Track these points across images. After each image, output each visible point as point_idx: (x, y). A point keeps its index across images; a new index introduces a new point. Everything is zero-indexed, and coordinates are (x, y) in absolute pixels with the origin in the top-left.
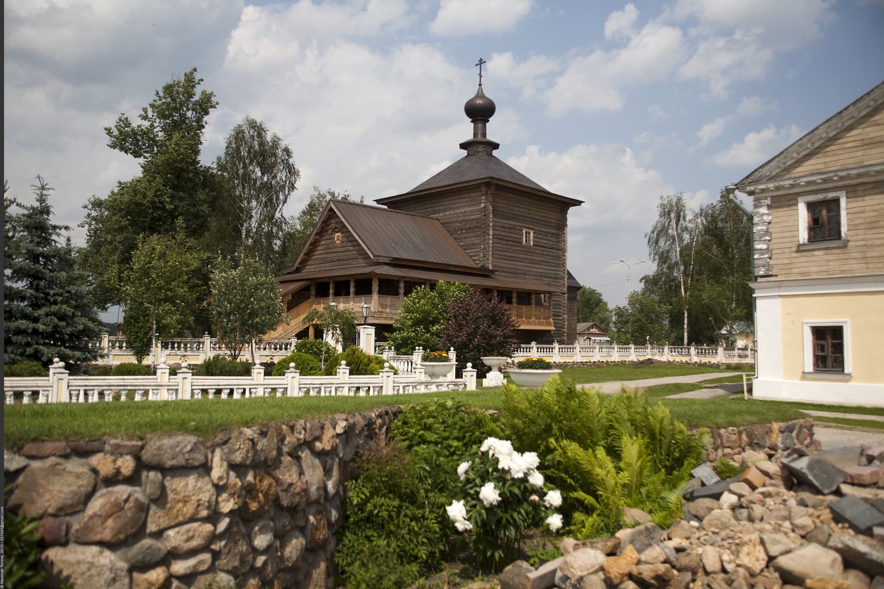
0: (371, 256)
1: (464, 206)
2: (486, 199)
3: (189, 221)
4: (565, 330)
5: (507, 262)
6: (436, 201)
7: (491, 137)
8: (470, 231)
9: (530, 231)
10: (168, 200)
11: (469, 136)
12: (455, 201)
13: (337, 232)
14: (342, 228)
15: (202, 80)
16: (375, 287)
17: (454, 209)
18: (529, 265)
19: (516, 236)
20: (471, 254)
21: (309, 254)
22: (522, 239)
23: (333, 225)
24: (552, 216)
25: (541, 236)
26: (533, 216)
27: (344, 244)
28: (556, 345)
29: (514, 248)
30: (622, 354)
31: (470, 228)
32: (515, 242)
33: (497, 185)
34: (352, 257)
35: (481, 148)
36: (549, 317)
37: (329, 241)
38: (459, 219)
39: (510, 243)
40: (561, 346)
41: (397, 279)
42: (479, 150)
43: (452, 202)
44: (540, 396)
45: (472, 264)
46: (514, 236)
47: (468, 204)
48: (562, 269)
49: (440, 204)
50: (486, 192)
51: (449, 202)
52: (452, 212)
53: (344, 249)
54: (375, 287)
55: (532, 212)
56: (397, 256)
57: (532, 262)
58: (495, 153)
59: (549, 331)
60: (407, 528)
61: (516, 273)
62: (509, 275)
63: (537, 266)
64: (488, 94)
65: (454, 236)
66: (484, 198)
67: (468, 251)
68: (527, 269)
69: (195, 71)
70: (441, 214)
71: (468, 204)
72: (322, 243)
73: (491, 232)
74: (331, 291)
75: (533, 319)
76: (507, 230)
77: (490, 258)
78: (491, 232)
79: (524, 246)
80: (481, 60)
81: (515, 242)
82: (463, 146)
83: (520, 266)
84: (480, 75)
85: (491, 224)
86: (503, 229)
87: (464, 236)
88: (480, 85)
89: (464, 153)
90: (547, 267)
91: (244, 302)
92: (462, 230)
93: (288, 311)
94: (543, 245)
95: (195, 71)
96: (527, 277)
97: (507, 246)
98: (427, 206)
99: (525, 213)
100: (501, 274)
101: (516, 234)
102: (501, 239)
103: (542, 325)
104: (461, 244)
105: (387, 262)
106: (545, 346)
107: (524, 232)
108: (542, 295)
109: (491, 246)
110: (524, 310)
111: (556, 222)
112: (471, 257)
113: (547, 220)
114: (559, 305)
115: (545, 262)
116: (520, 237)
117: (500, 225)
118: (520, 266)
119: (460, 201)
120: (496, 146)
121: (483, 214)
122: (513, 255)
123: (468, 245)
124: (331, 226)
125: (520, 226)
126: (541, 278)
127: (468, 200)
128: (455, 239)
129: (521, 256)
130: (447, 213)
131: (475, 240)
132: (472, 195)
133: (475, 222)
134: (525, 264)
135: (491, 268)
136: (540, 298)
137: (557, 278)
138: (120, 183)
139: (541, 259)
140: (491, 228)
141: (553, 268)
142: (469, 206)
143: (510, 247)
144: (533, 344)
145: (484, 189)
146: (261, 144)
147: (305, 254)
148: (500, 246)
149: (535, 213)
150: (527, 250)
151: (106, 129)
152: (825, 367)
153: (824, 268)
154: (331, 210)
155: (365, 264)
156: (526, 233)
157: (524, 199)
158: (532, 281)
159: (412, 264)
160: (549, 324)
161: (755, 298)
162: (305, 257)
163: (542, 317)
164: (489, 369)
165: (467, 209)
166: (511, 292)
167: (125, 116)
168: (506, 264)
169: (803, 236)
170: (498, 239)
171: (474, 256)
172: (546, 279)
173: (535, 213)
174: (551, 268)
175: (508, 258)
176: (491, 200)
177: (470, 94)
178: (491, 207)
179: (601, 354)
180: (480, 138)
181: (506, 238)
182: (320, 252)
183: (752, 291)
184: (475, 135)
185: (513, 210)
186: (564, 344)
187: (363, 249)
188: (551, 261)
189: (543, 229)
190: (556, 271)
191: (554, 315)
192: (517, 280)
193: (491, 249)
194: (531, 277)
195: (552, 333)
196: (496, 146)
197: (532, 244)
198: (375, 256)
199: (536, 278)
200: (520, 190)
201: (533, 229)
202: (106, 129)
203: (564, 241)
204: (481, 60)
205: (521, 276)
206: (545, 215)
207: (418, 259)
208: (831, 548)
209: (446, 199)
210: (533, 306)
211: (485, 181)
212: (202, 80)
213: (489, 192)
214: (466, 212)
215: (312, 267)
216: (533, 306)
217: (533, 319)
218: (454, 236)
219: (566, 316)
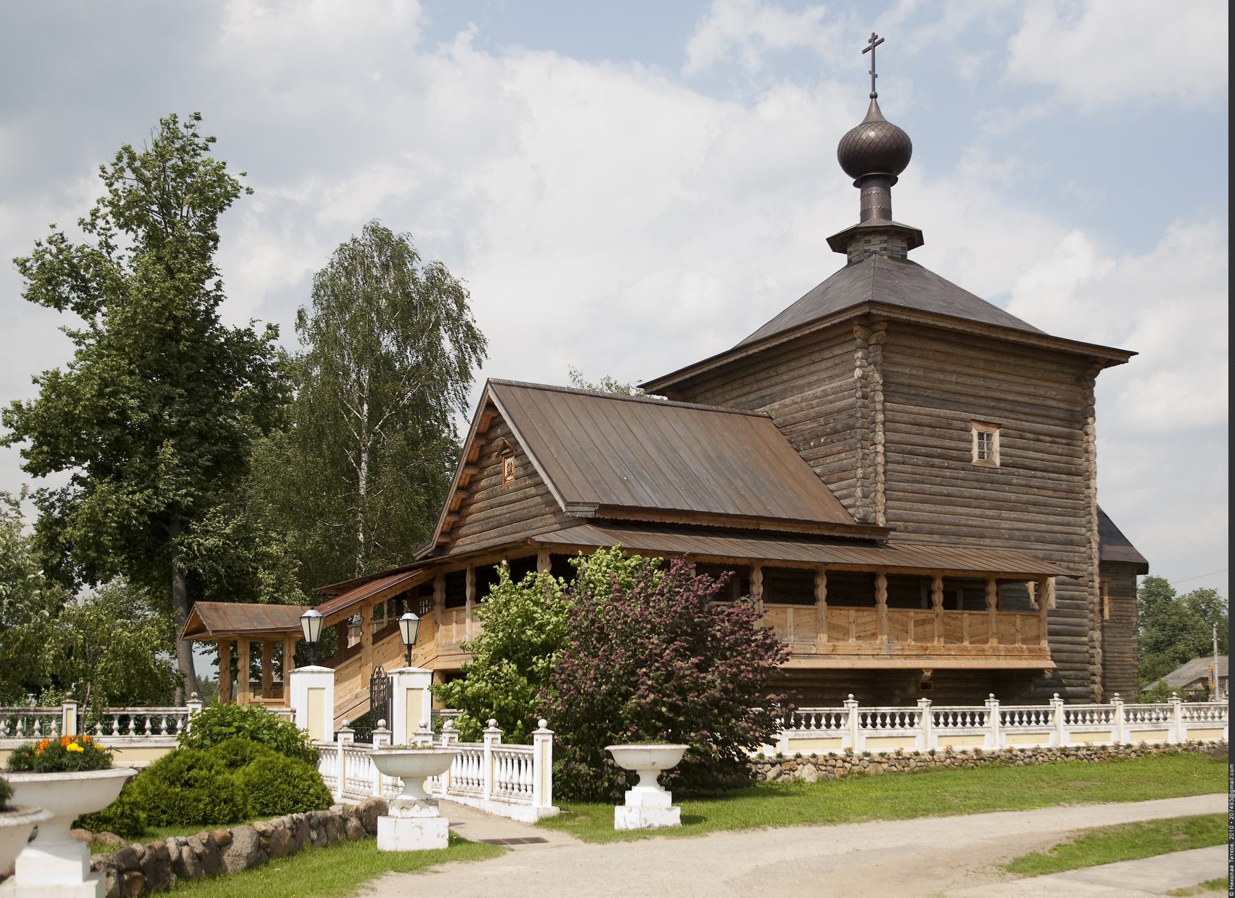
0: (561, 504)
1: (820, 381)
2: (865, 358)
4: (1097, 668)
5: (927, 506)
6: (764, 374)
7: (901, 216)
8: (835, 437)
9: (990, 430)
10: (133, 403)
11: (848, 216)
12: (804, 371)
13: (507, 456)
14: (512, 449)
15: (213, 140)
17: (801, 389)
18: (991, 513)
19: (953, 444)
20: (837, 494)
21: (460, 511)
22: (970, 450)
23: (499, 442)
24: (1052, 393)
25: (1020, 442)
26: (998, 395)
27: (521, 483)
28: (1057, 706)
29: (948, 473)
30: (1199, 725)
31: (836, 432)
32: (952, 458)
33: (891, 321)
34: (533, 511)
35: (876, 244)
36: (1038, 638)
37: (494, 479)
38: (812, 412)
39: (937, 461)
40: (869, 710)
41: (747, 562)
42: (873, 248)
43: (795, 374)
45: (840, 517)
46: (947, 443)
47: (829, 373)
48: (1084, 521)
49: (773, 381)
50: (866, 340)
51: (791, 374)
52: (797, 398)
53: (520, 494)
55: (995, 384)
57: (999, 504)
58: (913, 255)
59: (1040, 672)
61: (955, 534)
62: (936, 538)
63: (1013, 515)
65: (803, 453)
66: (859, 354)
67: (832, 487)
68: (987, 522)
69: (198, 118)
70: (776, 405)
71: (829, 373)
72: (483, 483)
73: (880, 437)
75: (993, 642)
76: (927, 430)
77: (880, 498)
78: (880, 437)
79: (975, 469)
80: (875, 37)
81: (952, 458)
82: (839, 243)
83: (964, 515)
84: (875, 76)
85: (880, 417)
86: (915, 429)
87: (822, 450)
88: (874, 96)
89: (841, 260)
90: (1043, 517)
92: (818, 437)
93: (373, 644)
94: (1028, 462)
95: (198, 118)
96: (988, 541)
97: (928, 470)
98: (747, 389)
99: (975, 386)
100: (913, 536)
101: (951, 439)
102: (910, 453)
103: (1020, 657)
104: (818, 470)
105: (590, 515)
106: (1024, 708)
107: (975, 433)
108: (1031, 585)
109: (880, 469)
110: (966, 623)
111: (1062, 405)
112: (838, 499)
113: (1040, 401)
114: (1078, 607)
115: (1034, 504)
116: (962, 445)
117: (906, 417)
118: (964, 515)
119: (813, 368)
120: (914, 238)
121: (859, 394)
122: (945, 490)
123: (832, 472)
124: (495, 444)
125: (962, 420)
126: (1027, 544)
127: (829, 363)
128: (806, 460)
129: (967, 492)
130: (787, 401)
131: (846, 459)
132: (837, 351)
133: (844, 415)
134: (978, 511)
135: (881, 522)
136: (1026, 591)
137: (1071, 543)
138: (130, 146)
139: (1024, 497)
140: (880, 427)
141: (1060, 519)
142: (831, 378)
143: (936, 471)
144: (923, 705)
145: (859, 332)
146: (402, 282)
147: (450, 513)
148: (908, 468)
149: (1005, 386)
150: (986, 477)
154: (490, 405)
155: (557, 526)
156: (981, 435)
157: (972, 353)
158: (1001, 551)
159: (657, 519)
160: (1039, 654)
162: (453, 519)
163: (1019, 637)
164: (633, 778)
165: (828, 387)
166: (929, 579)
167: (58, 230)
168: (926, 512)
170: (903, 452)
171: (845, 497)
172: (1039, 546)
173: (1005, 386)
174: (1052, 518)
175: (932, 499)
176: (879, 359)
178: (877, 377)
179: (1133, 726)
180: (875, 221)
181: (924, 450)
182: (480, 505)
184: (865, 214)
185: (942, 382)
186: (1094, 701)
187: (549, 492)
188: (1054, 501)
189: (1027, 425)
190: (1068, 524)
191: (1051, 633)
192: (960, 551)
193: (881, 477)
194: (999, 543)
195: (1048, 675)
196: (914, 238)
197: (998, 463)
198: (568, 504)
199: (1013, 543)
200: (908, 324)
201: (999, 426)
203: (1086, 451)
204: (875, 37)
205: (970, 540)
206: (1032, 390)
207: (686, 508)
209: (783, 368)
210: (993, 610)
211: (858, 313)
212: (213, 140)
213: (873, 341)
214: (825, 394)
215: (467, 540)
216: (993, 610)
217: (993, 642)
218: (803, 453)
219: (1097, 635)
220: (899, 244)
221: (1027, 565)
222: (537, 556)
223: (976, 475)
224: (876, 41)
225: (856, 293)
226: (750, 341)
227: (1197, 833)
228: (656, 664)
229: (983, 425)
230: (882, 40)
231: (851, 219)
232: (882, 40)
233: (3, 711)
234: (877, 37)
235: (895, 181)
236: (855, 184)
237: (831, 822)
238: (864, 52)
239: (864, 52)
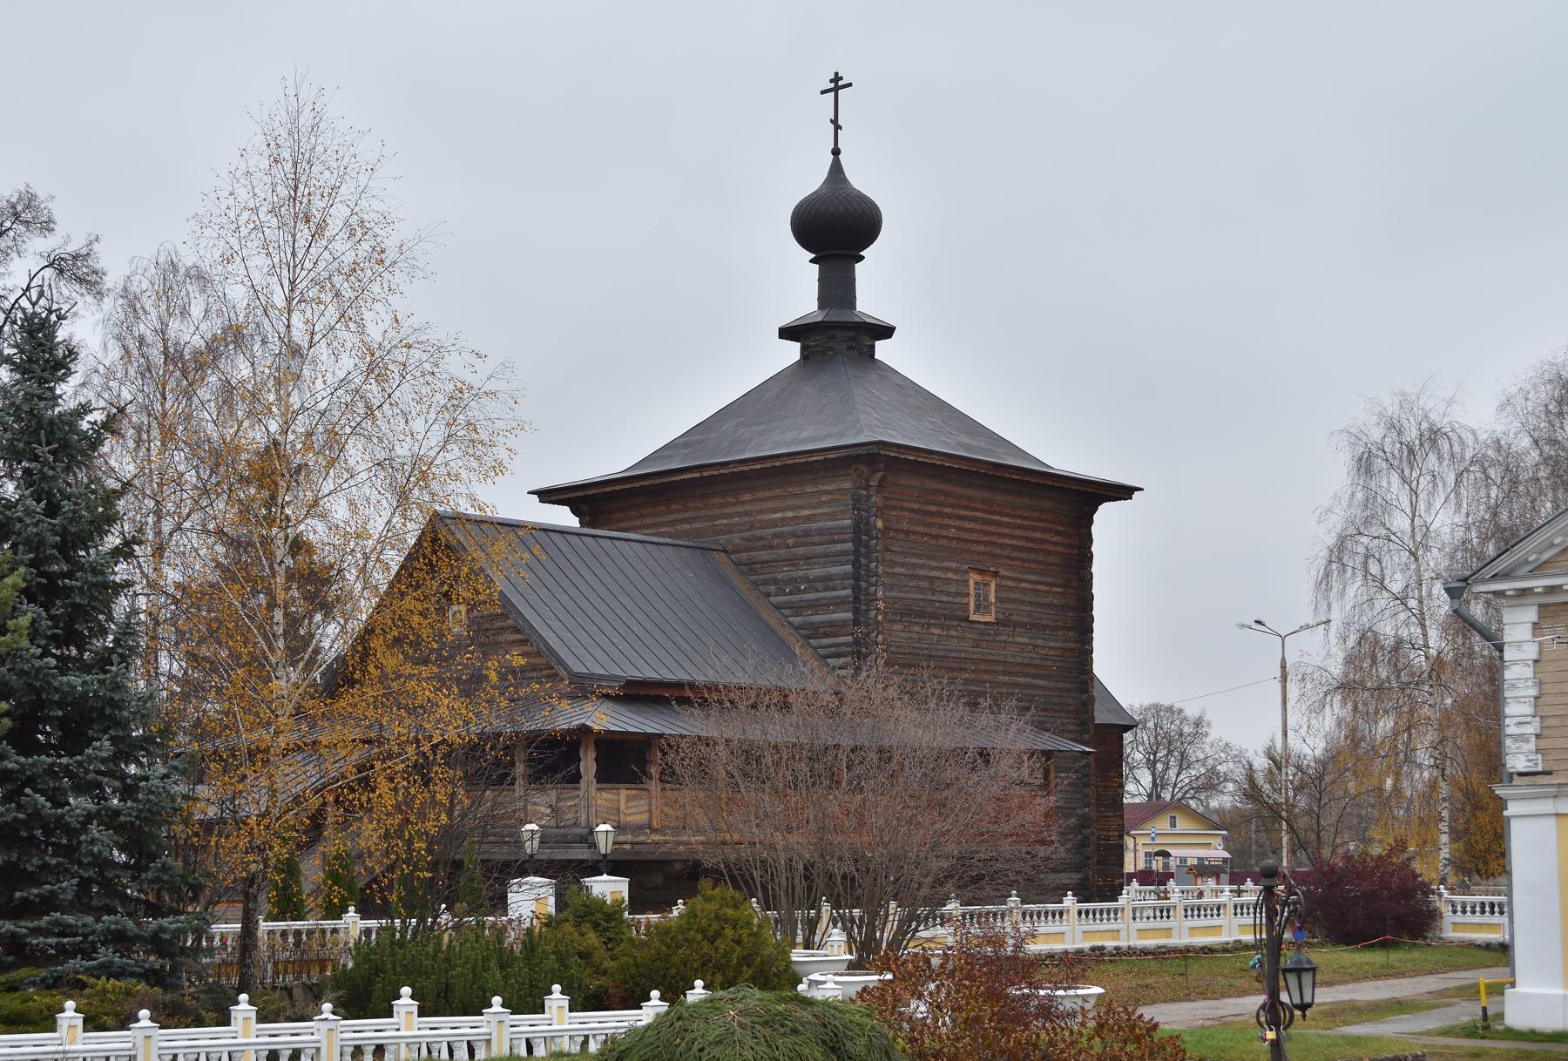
16: (588, 765)
54: (588, 765)
56: (635, 674)
58: (883, 350)
64: (859, 178)
80: (837, 78)
88: (836, 152)
89: (791, 352)
107: (972, 583)
152: (222, 933)
153: (1251, 910)
161: (1508, 819)
177: (812, 180)
183: (1501, 803)
196: (886, 332)
202: (836, 74)
204: (837, 78)
210: (654, 786)
224: (840, 83)
230: (850, 85)
232: (850, 85)
234: (841, 78)
239: (823, 92)
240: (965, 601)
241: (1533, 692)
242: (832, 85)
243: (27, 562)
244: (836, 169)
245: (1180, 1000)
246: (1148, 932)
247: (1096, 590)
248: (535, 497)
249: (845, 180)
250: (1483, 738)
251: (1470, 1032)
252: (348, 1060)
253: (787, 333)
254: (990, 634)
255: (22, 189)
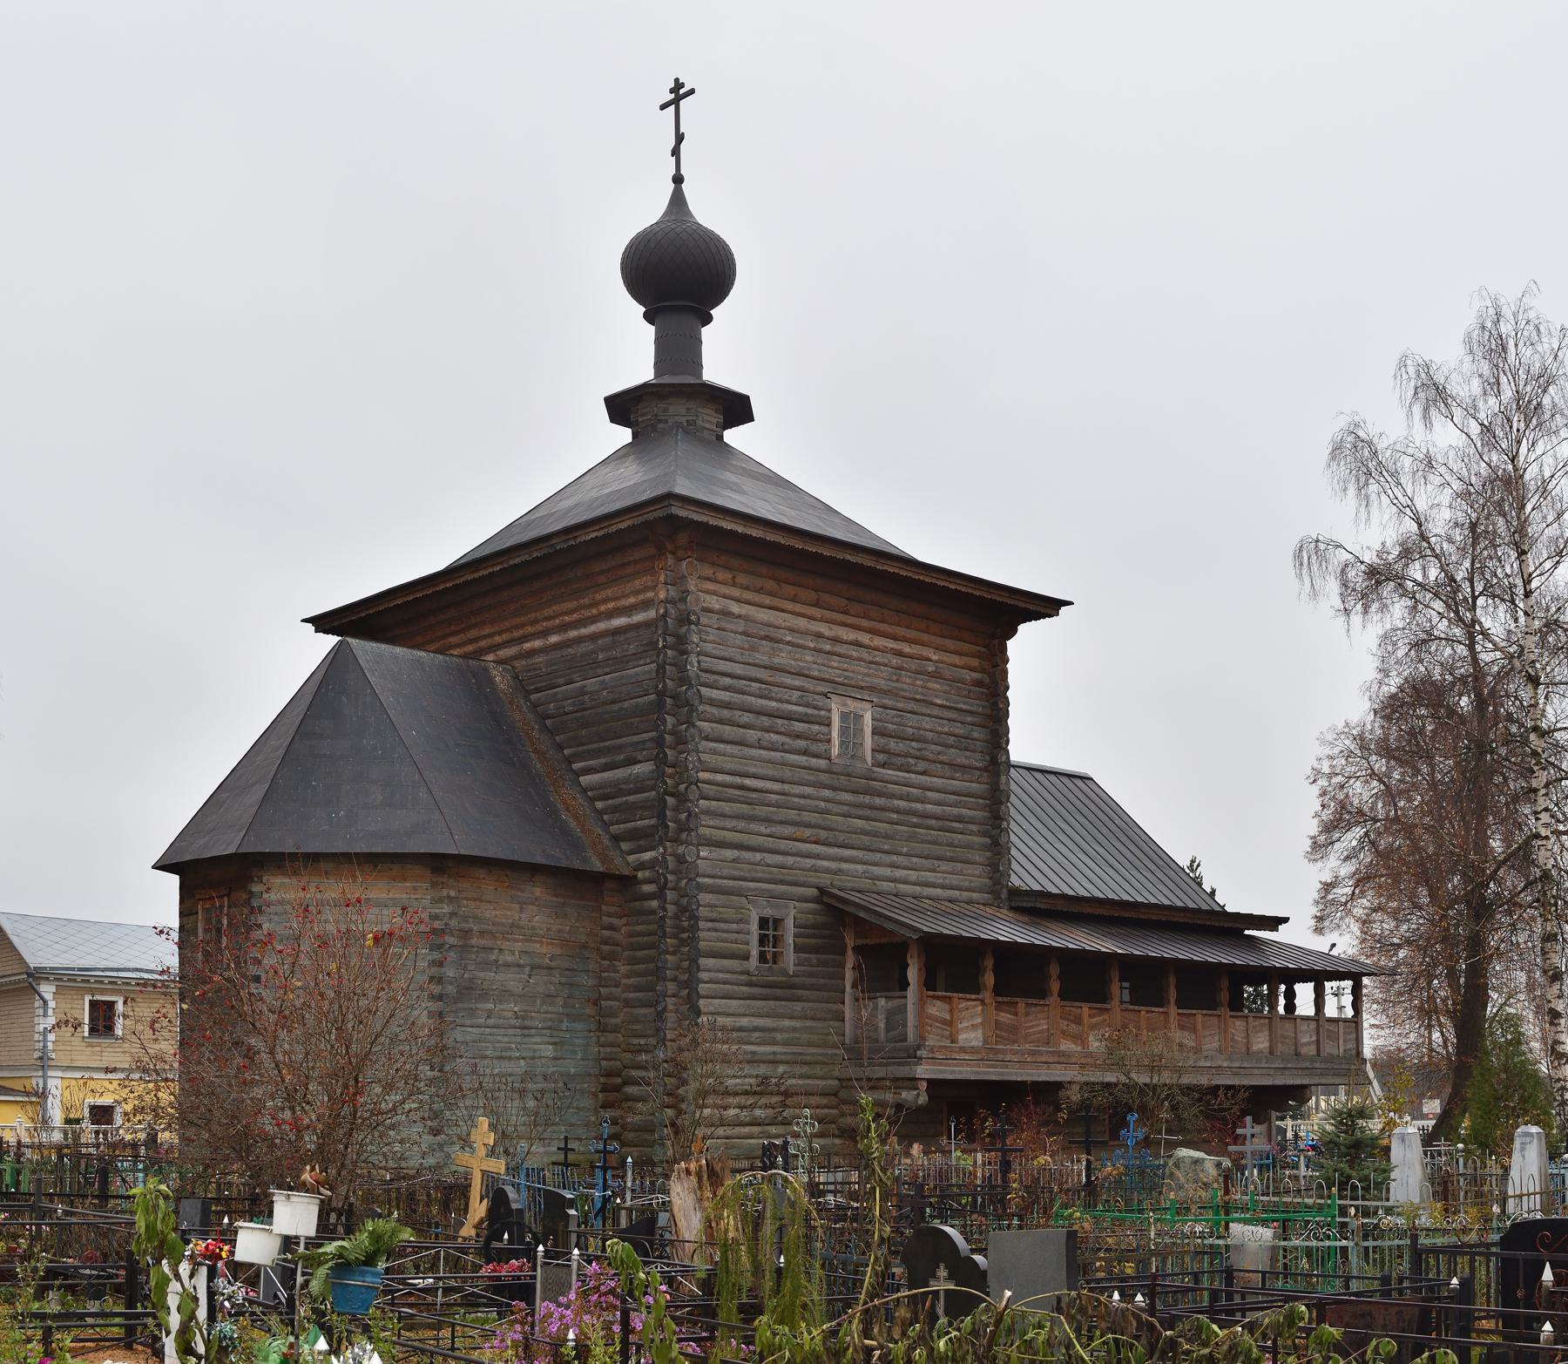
3: (1402, 691)
35: (678, 410)
44: (1361, 740)
60: (1330, 897)
64: (706, 212)
74: (1055, 986)
80: (678, 85)
82: (621, 407)
88: (678, 179)
89: (624, 435)
91: (612, 1323)
151: (677, 80)
156: (844, 716)
169: (86, 1034)
177: (649, 211)
196: (737, 409)
202: (677, 80)
204: (678, 85)
208: (952, 1017)
210: (1054, 999)
220: (708, 417)
221: (914, 918)
222: (721, 1360)
223: (741, 764)
224: (682, 91)
225: (635, 483)
226: (487, 551)
227: (1227, 1198)
228: (787, 1328)
229: (714, 669)
230: (692, 92)
231: (643, 372)
232: (692, 92)
233: (186, 1349)
234: (682, 85)
235: (707, 319)
236: (649, 317)
237: (180, 913)
238: (663, 107)
239: (663, 107)
240: (561, 1245)
241: (1249, 1128)
242: (673, 96)
243: (47, 990)
244: (678, 201)
245: (467, 1205)
246: (721, 995)
247: (1011, 679)
248: (310, 627)
249: (689, 213)
250: (1410, 584)
251: (576, 537)
252: (1567, 1165)
253: (322, 623)
254: (511, 1049)
255: (1320, 886)
